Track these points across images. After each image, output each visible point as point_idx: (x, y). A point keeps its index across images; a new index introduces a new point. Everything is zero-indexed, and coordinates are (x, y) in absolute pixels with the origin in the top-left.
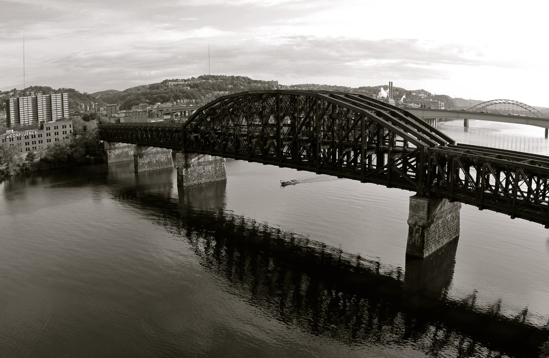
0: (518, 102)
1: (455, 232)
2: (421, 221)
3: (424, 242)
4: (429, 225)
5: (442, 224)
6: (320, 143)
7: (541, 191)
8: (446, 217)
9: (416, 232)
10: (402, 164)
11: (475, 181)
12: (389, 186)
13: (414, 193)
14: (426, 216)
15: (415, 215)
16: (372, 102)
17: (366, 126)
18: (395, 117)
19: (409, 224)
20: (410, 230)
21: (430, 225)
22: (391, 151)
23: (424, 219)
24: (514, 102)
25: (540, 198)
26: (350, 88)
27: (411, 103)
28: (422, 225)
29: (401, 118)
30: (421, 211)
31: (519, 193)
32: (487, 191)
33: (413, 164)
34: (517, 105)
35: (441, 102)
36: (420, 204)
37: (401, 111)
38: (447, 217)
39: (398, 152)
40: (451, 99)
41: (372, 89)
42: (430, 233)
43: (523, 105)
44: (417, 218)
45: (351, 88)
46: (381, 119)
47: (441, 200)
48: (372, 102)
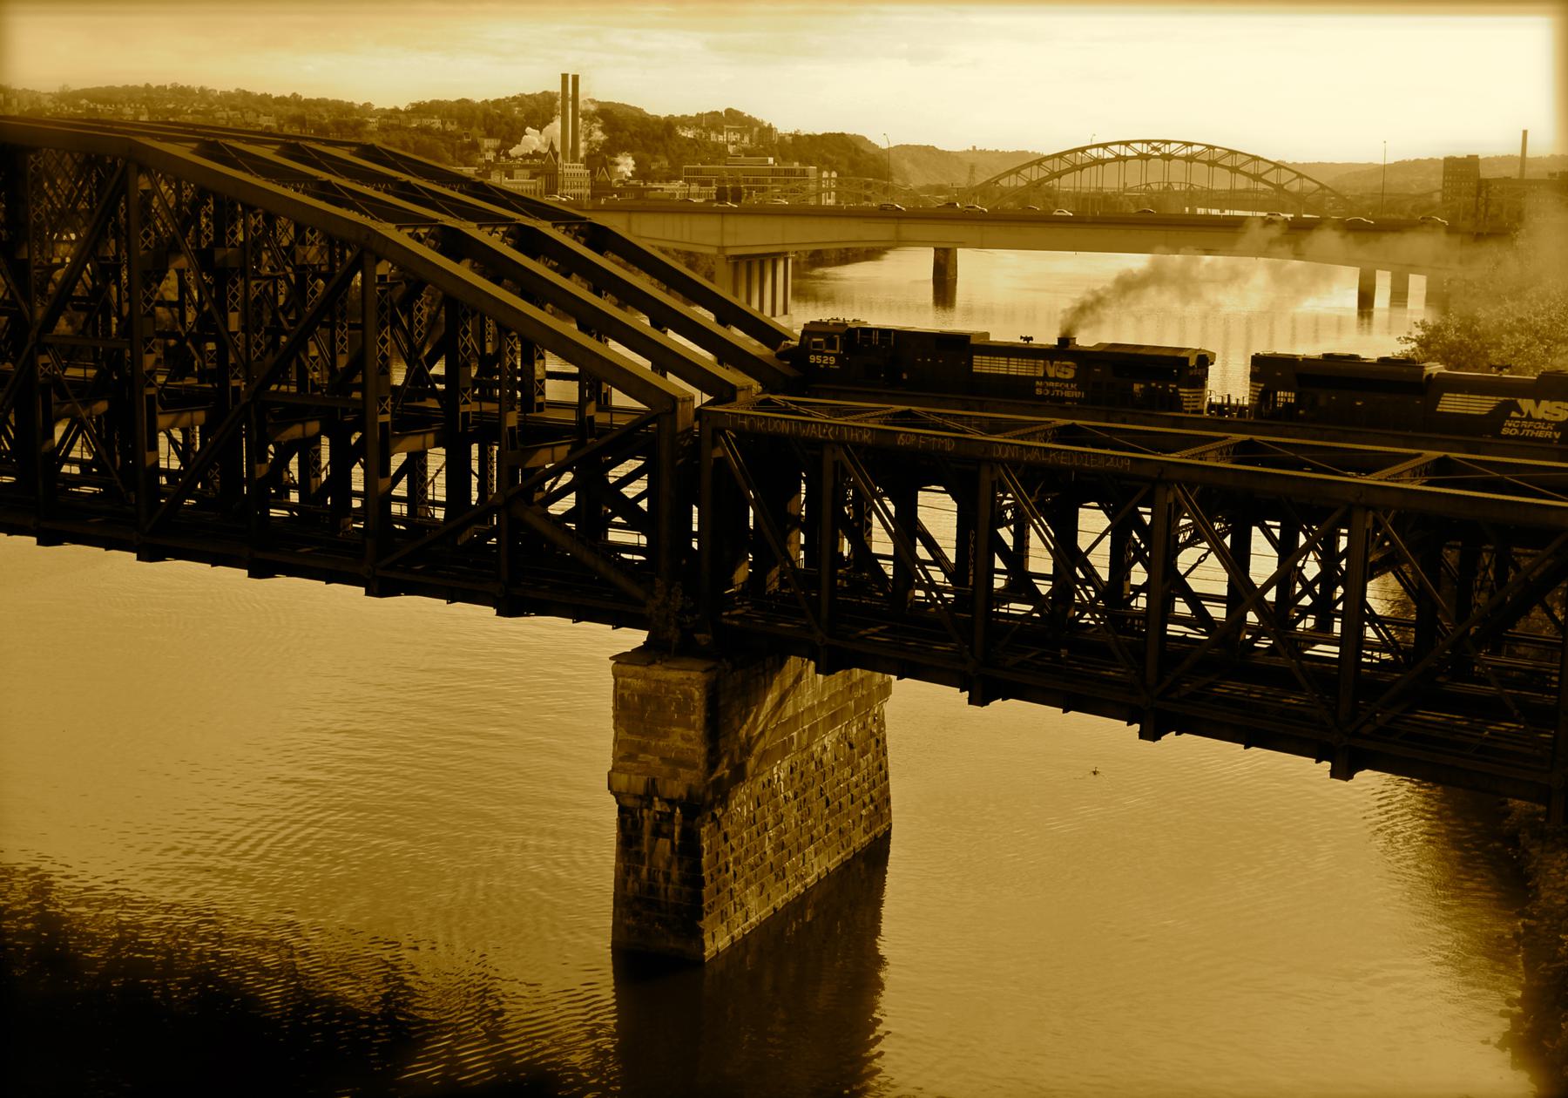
0: (1213, 147)
1: (868, 816)
2: (675, 776)
3: (701, 883)
4: (722, 793)
5: (792, 780)
6: (151, 398)
7: (1308, 588)
8: (809, 746)
9: (657, 833)
10: (573, 496)
11: (953, 560)
12: (510, 607)
13: (635, 638)
14: (702, 750)
15: (644, 749)
16: (423, 183)
17: (382, 308)
18: (534, 257)
19: (617, 795)
20: (622, 822)
21: (728, 792)
22: (512, 429)
23: (694, 766)
24: (1196, 149)
25: (1301, 625)
26: (367, 106)
27: (668, 180)
28: (685, 795)
29: (569, 263)
30: (671, 723)
31: (1181, 608)
32: (1012, 605)
33: (630, 491)
34: (1212, 163)
35: (820, 171)
36: (667, 689)
37: (568, 225)
38: (814, 748)
39: (553, 433)
40: (871, 151)
41: (478, 112)
42: (731, 835)
43: (1240, 161)
45: (375, 107)
46: (463, 270)
47: (781, 665)
48: (423, 183)
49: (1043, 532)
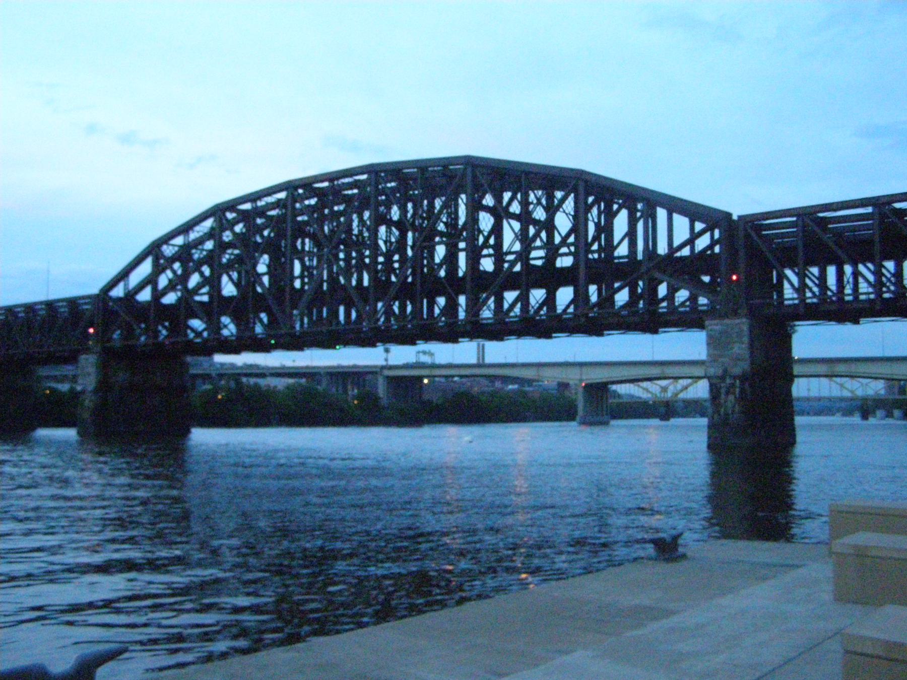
15: (721, 356)
44: (726, 360)
49: (650, 230)
